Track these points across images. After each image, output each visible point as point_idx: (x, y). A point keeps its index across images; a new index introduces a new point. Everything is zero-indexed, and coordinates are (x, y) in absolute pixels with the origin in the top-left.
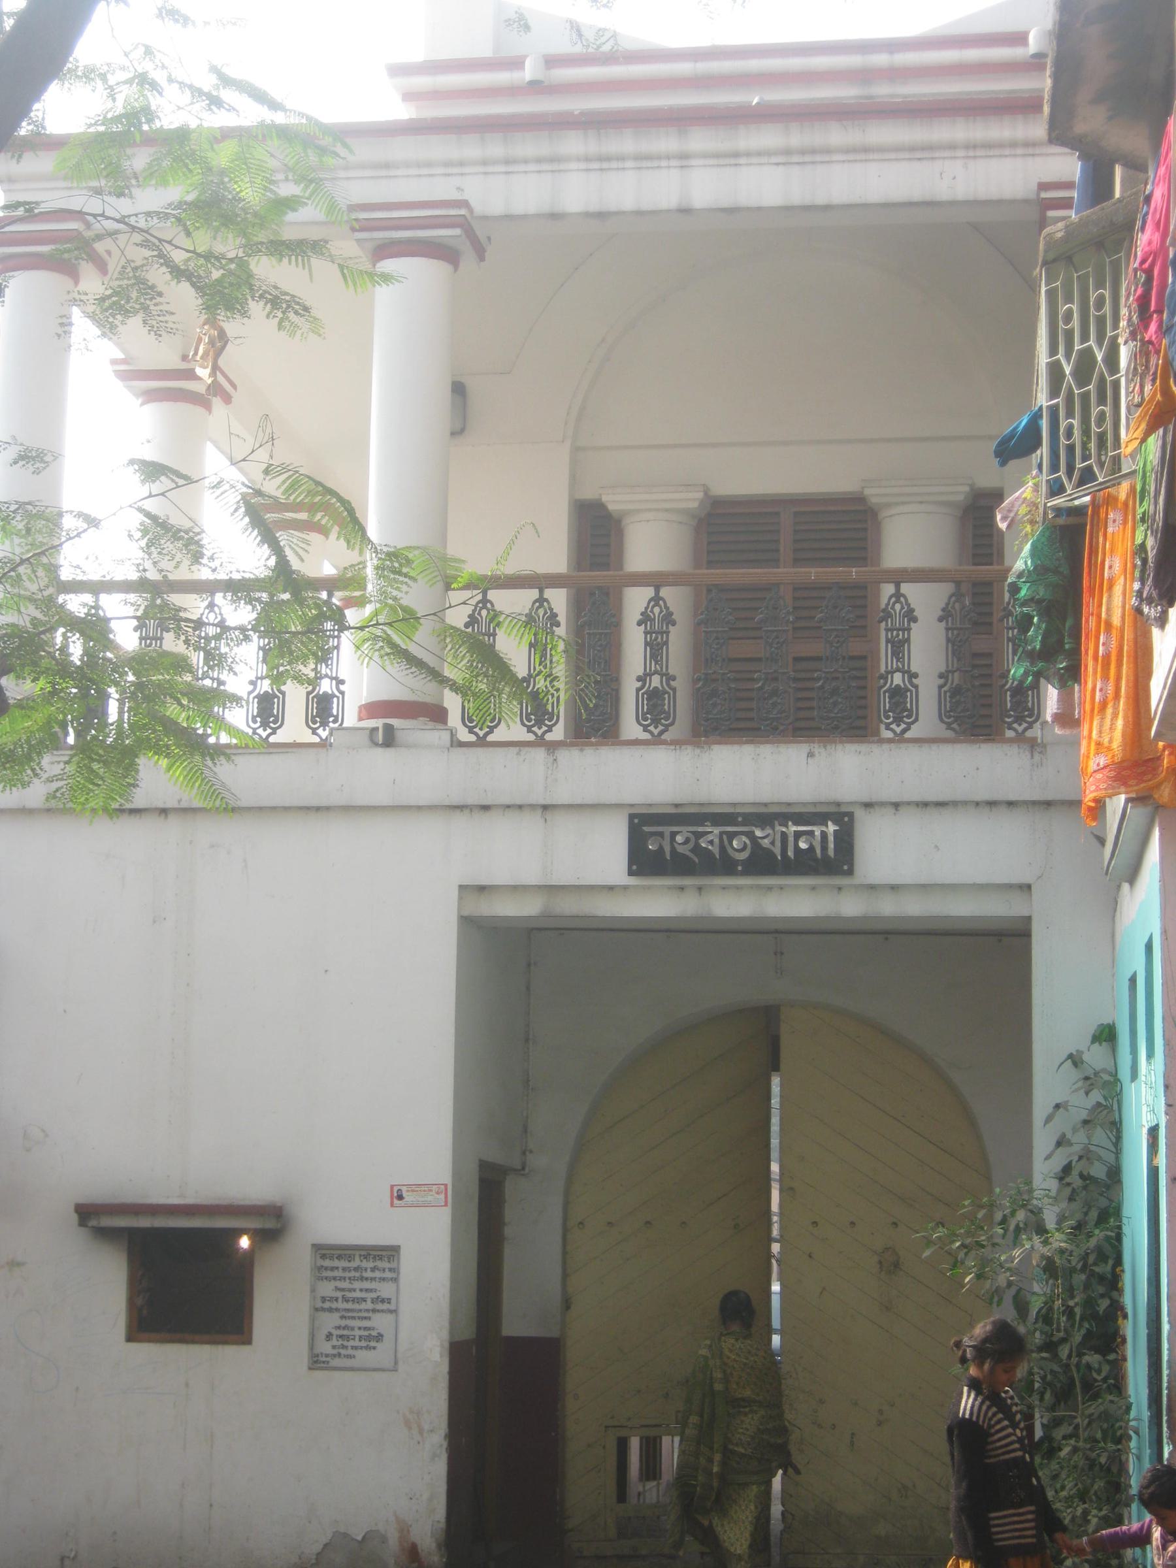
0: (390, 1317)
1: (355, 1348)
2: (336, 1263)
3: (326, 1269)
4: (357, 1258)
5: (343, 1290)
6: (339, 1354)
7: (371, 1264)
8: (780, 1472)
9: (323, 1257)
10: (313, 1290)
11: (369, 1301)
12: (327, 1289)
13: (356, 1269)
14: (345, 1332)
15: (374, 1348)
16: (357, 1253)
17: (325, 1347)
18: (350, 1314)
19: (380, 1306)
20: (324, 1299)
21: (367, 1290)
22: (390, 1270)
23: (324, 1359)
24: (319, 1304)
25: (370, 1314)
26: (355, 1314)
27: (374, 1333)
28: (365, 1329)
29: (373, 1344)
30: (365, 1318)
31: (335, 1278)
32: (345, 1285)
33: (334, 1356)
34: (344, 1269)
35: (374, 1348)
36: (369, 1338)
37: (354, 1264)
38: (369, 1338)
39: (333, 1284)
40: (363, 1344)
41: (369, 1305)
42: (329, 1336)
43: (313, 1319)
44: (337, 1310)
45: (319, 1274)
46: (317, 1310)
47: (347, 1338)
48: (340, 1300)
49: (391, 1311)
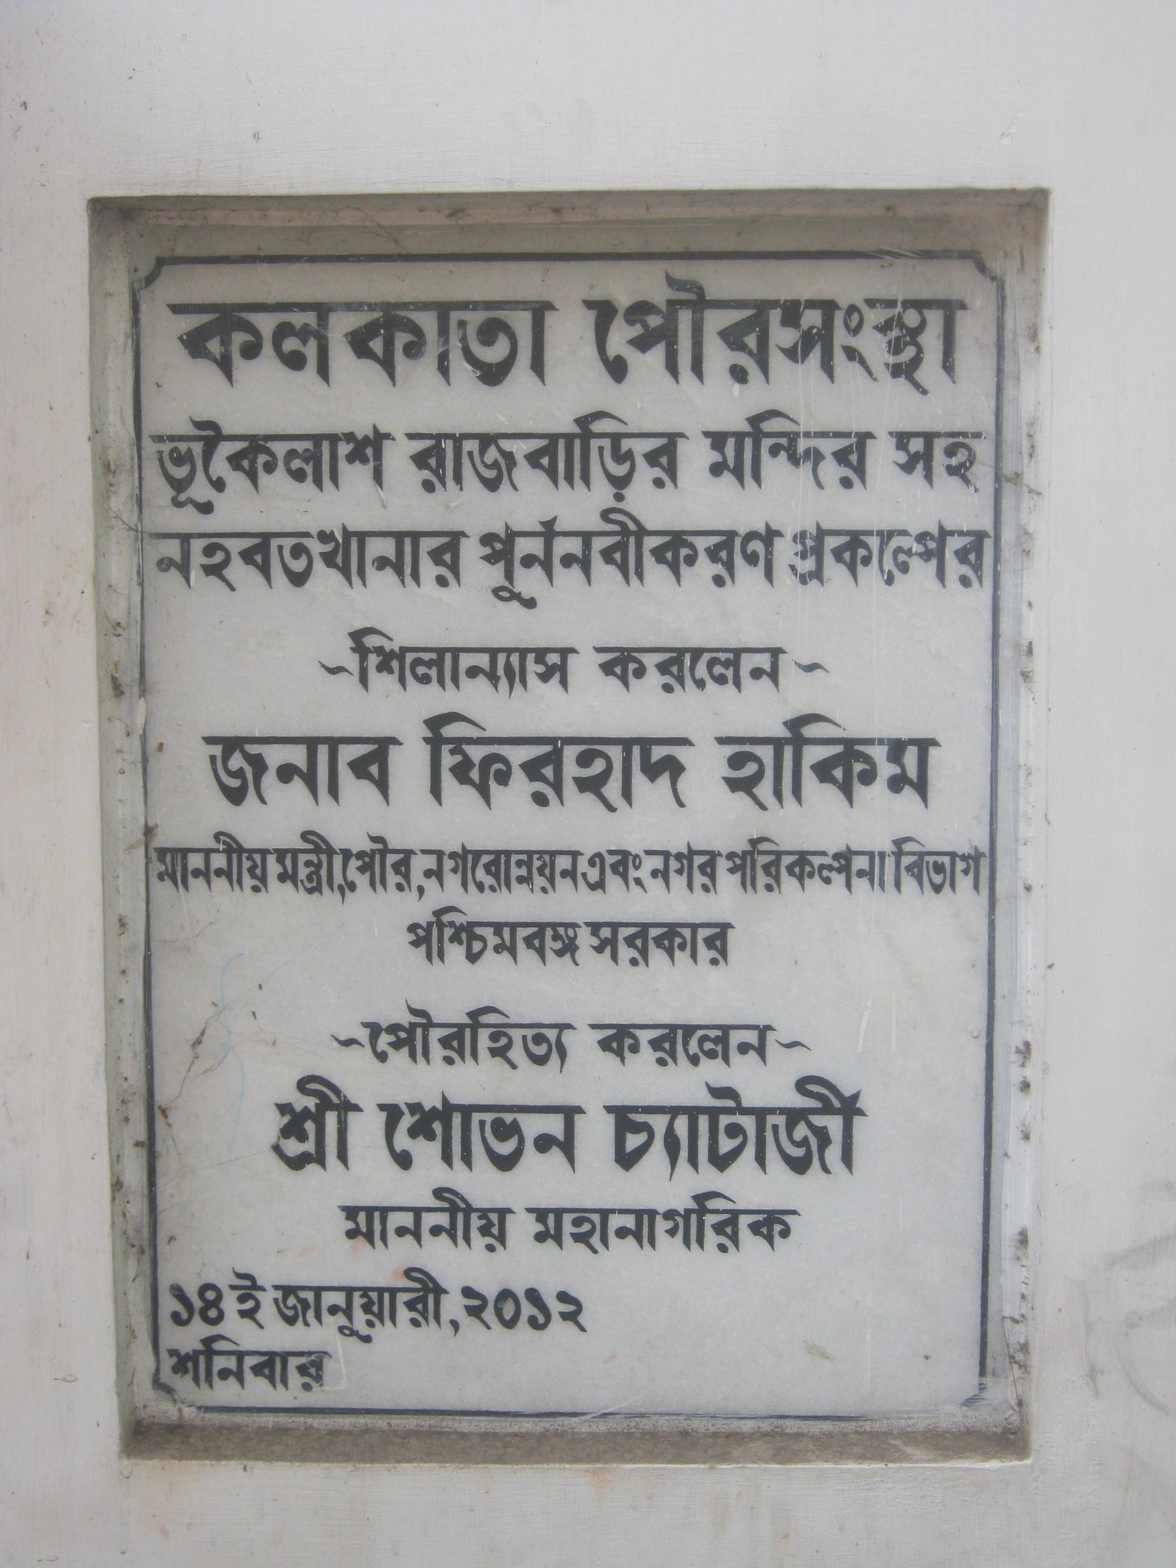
0: (931, 929)
1: (590, 1227)
2: (354, 396)
3: (253, 455)
4: (569, 332)
5: (436, 664)
6: (425, 1293)
7: (713, 401)
8: (217, 315)
9: (220, 336)
10: (128, 680)
11: (705, 767)
12: (266, 660)
13: (562, 454)
14: (475, 1081)
15: (772, 1224)
16: (568, 288)
17: (275, 1224)
18: (518, 904)
19: (818, 819)
20: (240, 765)
21: (677, 664)
22: (919, 452)
23: (273, 1334)
24: (197, 813)
25: (726, 900)
26: (570, 904)
27: (766, 1084)
28: (671, 1041)
29: (750, 1185)
30: (672, 937)
31: (345, 552)
32: (456, 611)
33: (376, 1303)
34: (437, 457)
35: (772, 1224)
36: (716, 1129)
37: (563, 389)
38: (716, 1129)
39: (335, 605)
40: (660, 1184)
41: (711, 813)
42: (312, 1122)
43: (142, 967)
44: (383, 862)
45: (179, 502)
46: (173, 865)
47: (501, 1133)
48: (409, 764)
49: (932, 869)
